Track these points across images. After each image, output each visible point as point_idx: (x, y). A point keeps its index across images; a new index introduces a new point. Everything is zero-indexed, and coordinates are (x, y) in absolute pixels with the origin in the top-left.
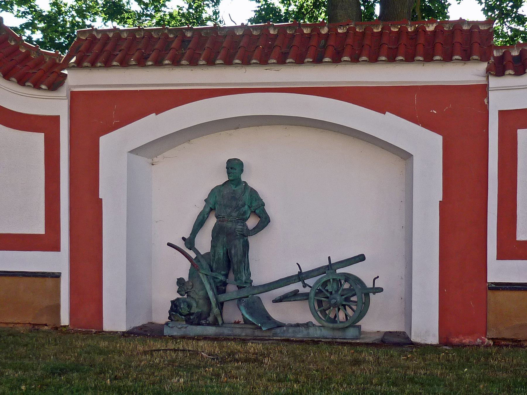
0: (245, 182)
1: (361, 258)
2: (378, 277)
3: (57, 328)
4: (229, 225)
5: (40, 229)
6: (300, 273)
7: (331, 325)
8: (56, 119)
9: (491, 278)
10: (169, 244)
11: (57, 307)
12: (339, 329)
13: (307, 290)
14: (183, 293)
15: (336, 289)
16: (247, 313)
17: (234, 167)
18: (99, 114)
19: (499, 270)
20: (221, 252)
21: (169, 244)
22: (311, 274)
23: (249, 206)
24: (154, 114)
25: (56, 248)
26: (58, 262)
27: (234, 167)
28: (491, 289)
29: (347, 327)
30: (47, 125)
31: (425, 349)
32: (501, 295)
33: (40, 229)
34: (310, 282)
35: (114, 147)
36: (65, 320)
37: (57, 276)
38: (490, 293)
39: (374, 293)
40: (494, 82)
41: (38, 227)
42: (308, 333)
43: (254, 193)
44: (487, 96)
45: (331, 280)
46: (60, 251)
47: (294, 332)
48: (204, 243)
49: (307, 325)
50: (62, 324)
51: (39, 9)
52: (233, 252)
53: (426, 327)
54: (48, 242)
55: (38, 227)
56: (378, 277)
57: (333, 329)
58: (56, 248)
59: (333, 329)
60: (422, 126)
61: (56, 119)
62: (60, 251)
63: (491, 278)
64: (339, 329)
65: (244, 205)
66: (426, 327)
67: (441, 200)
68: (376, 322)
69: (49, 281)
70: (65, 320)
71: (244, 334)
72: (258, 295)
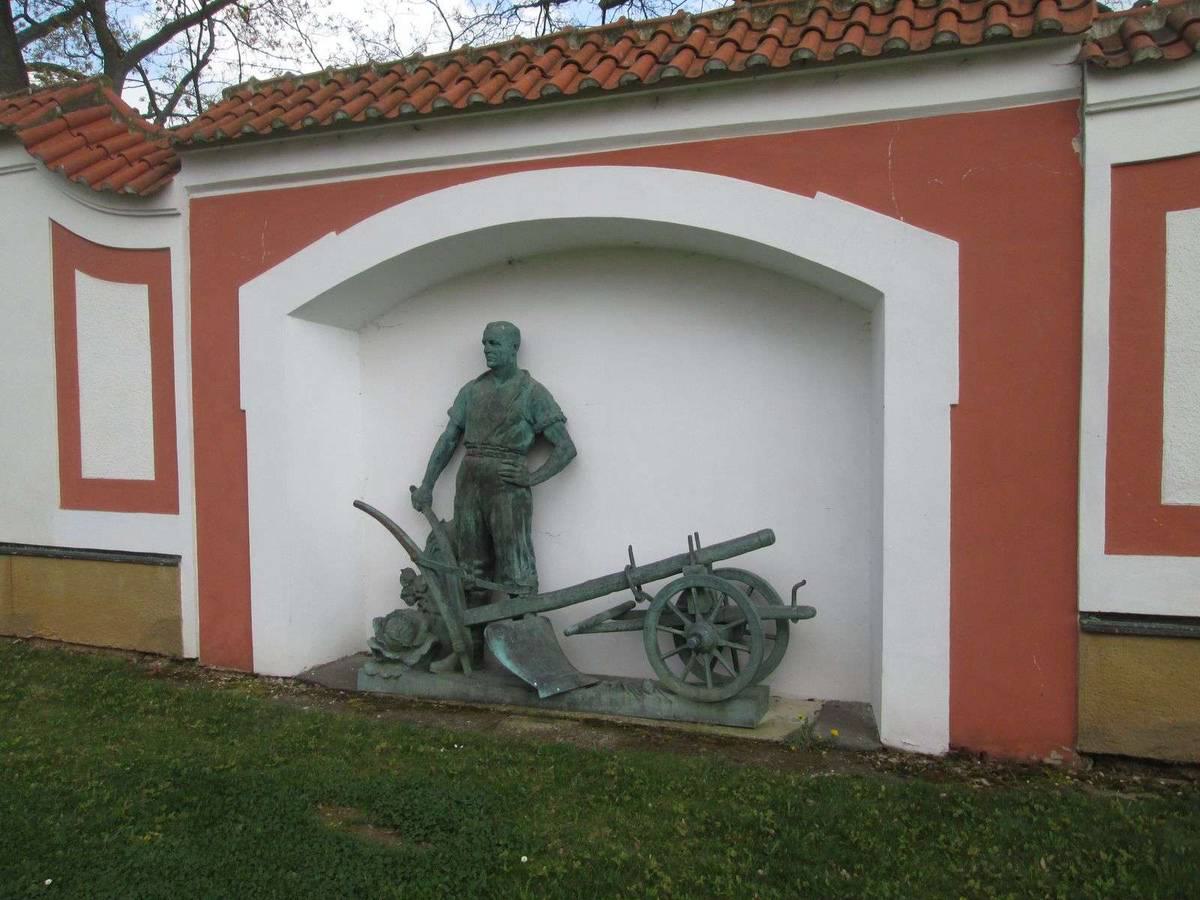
0: (526, 372)
1: (765, 539)
2: (804, 582)
3: (178, 660)
5: (146, 471)
6: (631, 568)
7: (693, 692)
9: (1091, 599)
10: (358, 505)
11: (176, 623)
12: (710, 703)
13: (644, 605)
14: (411, 598)
15: (714, 612)
16: (509, 658)
17: (502, 348)
18: (239, 242)
19: (1114, 581)
20: (470, 518)
21: (358, 505)
22: (654, 572)
23: (529, 422)
24: (333, 234)
25: (171, 506)
26: (173, 533)
28: (1090, 631)
29: (729, 700)
30: (147, 267)
32: (1117, 650)
33: (146, 471)
34: (652, 588)
35: (267, 302)
37: (173, 561)
38: (1085, 641)
40: (1097, 93)
41: (143, 469)
42: (643, 706)
43: (541, 399)
44: (1078, 131)
45: (693, 590)
46: (1109, 550)
48: (445, 504)
49: (637, 686)
50: (186, 656)
51: (221, 97)
52: (493, 520)
53: (916, 711)
54: (156, 496)
56: (804, 582)
57: (697, 701)
58: (171, 506)
59: (697, 701)
60: (906, 220)
62: (1109, 550)
63: (1091, 599)
64: (710, 703)
65: (516, 421)
66: (916, 711)
67: (957, 402)
68: (804, 683)
69: (163, 573)
70: (191, 647)
71: (508, 700)
72: (546, 614)
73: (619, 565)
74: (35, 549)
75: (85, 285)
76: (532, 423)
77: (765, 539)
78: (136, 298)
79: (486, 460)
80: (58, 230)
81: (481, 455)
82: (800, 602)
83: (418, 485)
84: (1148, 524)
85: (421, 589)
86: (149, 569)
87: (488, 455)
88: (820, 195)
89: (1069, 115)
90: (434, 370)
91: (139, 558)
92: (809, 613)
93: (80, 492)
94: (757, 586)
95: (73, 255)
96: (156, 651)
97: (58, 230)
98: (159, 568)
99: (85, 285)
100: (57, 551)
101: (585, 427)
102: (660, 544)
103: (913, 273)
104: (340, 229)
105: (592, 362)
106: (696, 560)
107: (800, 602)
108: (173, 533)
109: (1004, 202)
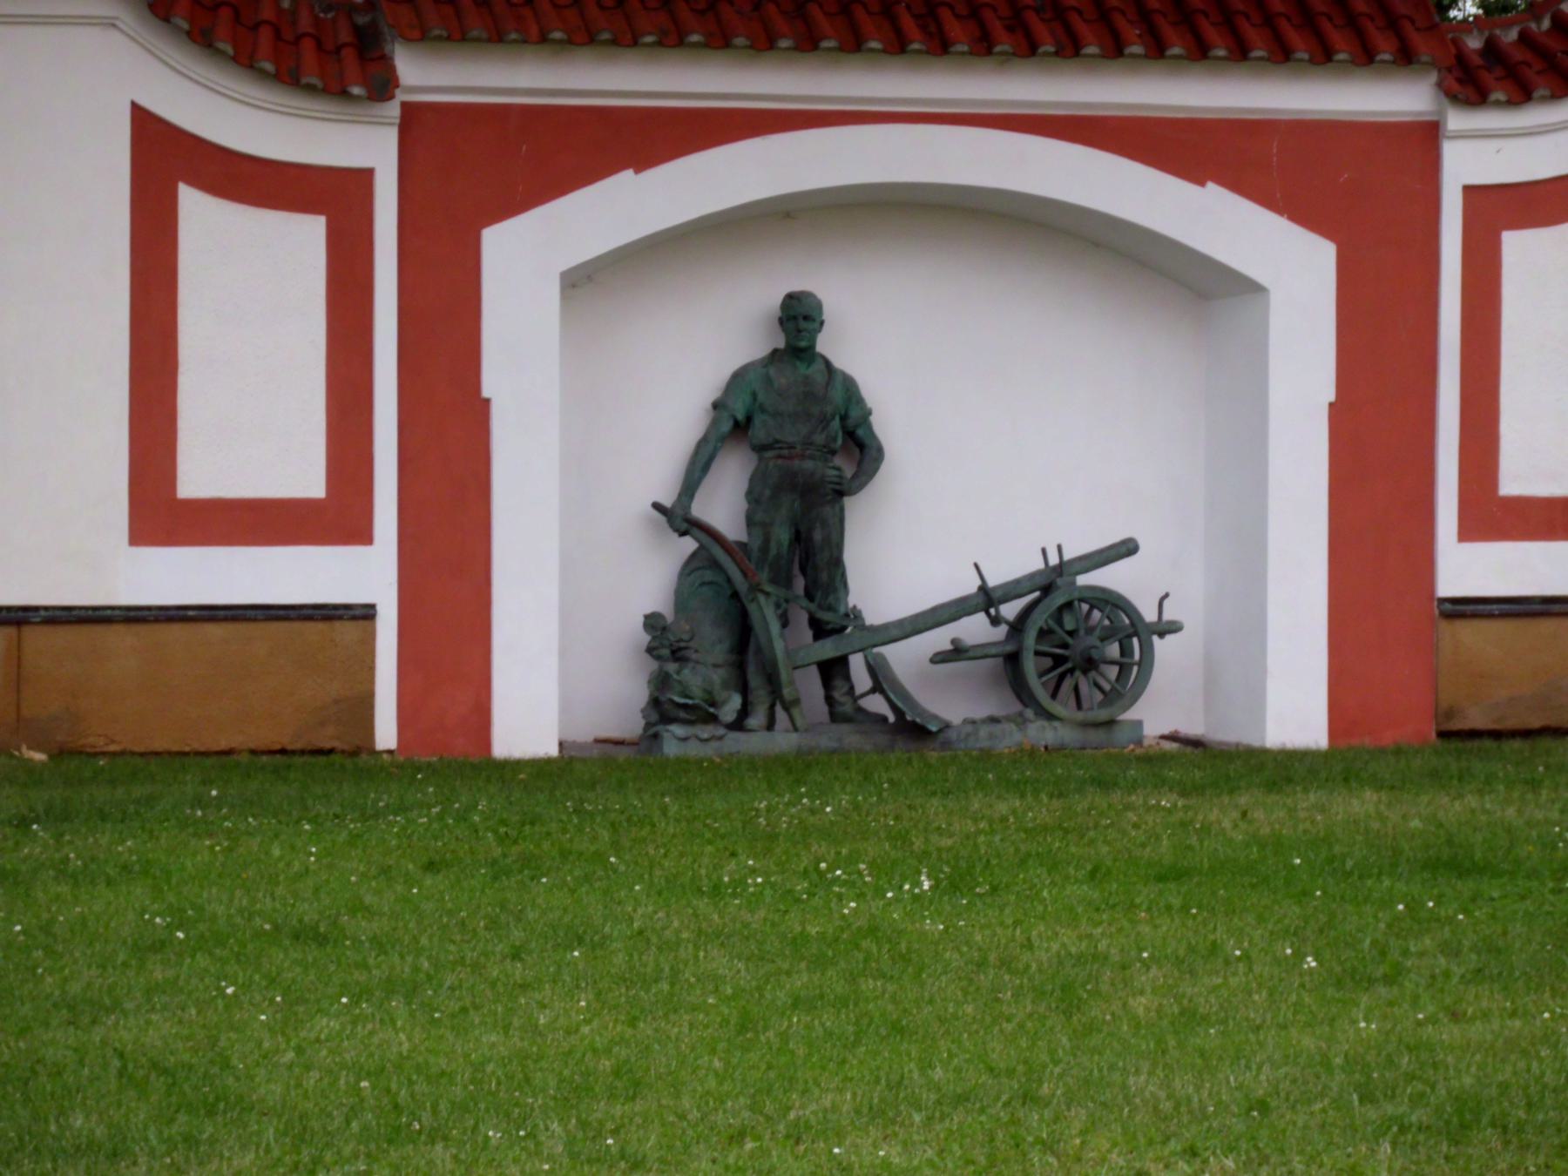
1: (1127, 548)
4: (808, 465)
6: (983, 589)
8: (363, 179)
11: (365, 703)
17: (799, 317)
19: (1467, 568)
22: (1011, 591)
25: (361, 533)
26: (366, 574)
27: (799, 317)
28: (1448, 616)
30: (335, 196)
31: (1285, 769)
32: (1470, 634)
35: (524, 258)
36: (386, 734)
37: (366, 614)
38: (1445, 627)
39: (1161, 635)
40: (1457, 120)
41: (305, 478)
47: (991, 736)
54: (336, 518)
55: (305, 478)
58: (361, 533)
61: (363, 179)
69: (346, 631)
70: (386, 734)
73: (970, 586)
74: (20, 614)
75: (198, 211)
76: (844, 418)
77: (1127, 548)
78: (304, 238)
79: (808, 465)
80: (145, 125)
81: (803, 457)
82: (1167, 616)
83: (668, 502)
84: (1492, 516)
85: (686, 637)
86: (321, 626)
87: (812, 457)
88: (1211, 185)
89: (1428, 135)
90: (704, 344)
91: (282, 612)
92: (1173, 628)
93: (161, 514)
94: (1109, 601)
95: (166, 160)
96: (327, 745)
97: (145, 125)
98: (337, 624)
99: (198, 211)
100: (83, 613)
101: (891, 421)
102: (1012, 563)
103: (1294, 270)
104: (637, 171)
105: (895, 338)
106: (1051, 581)
107: (1167, 616)
108: (366, 574)
109: (1365, 200)
